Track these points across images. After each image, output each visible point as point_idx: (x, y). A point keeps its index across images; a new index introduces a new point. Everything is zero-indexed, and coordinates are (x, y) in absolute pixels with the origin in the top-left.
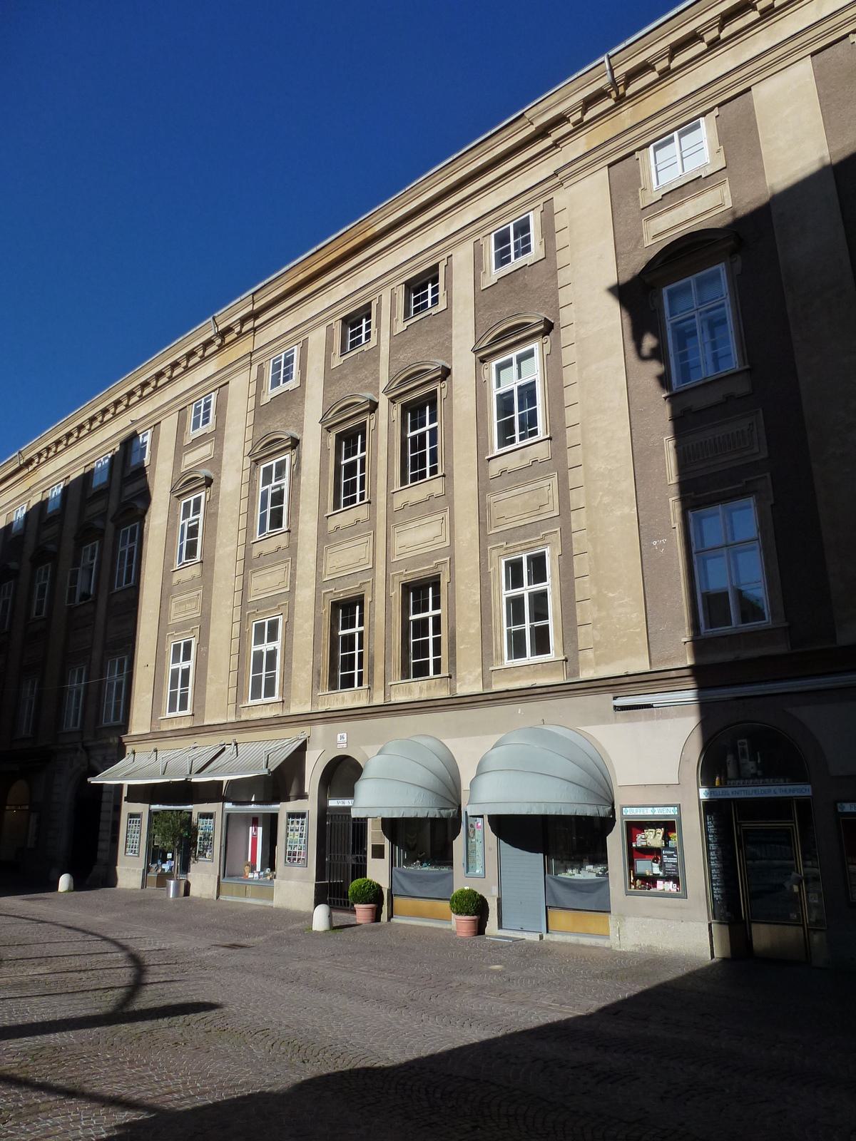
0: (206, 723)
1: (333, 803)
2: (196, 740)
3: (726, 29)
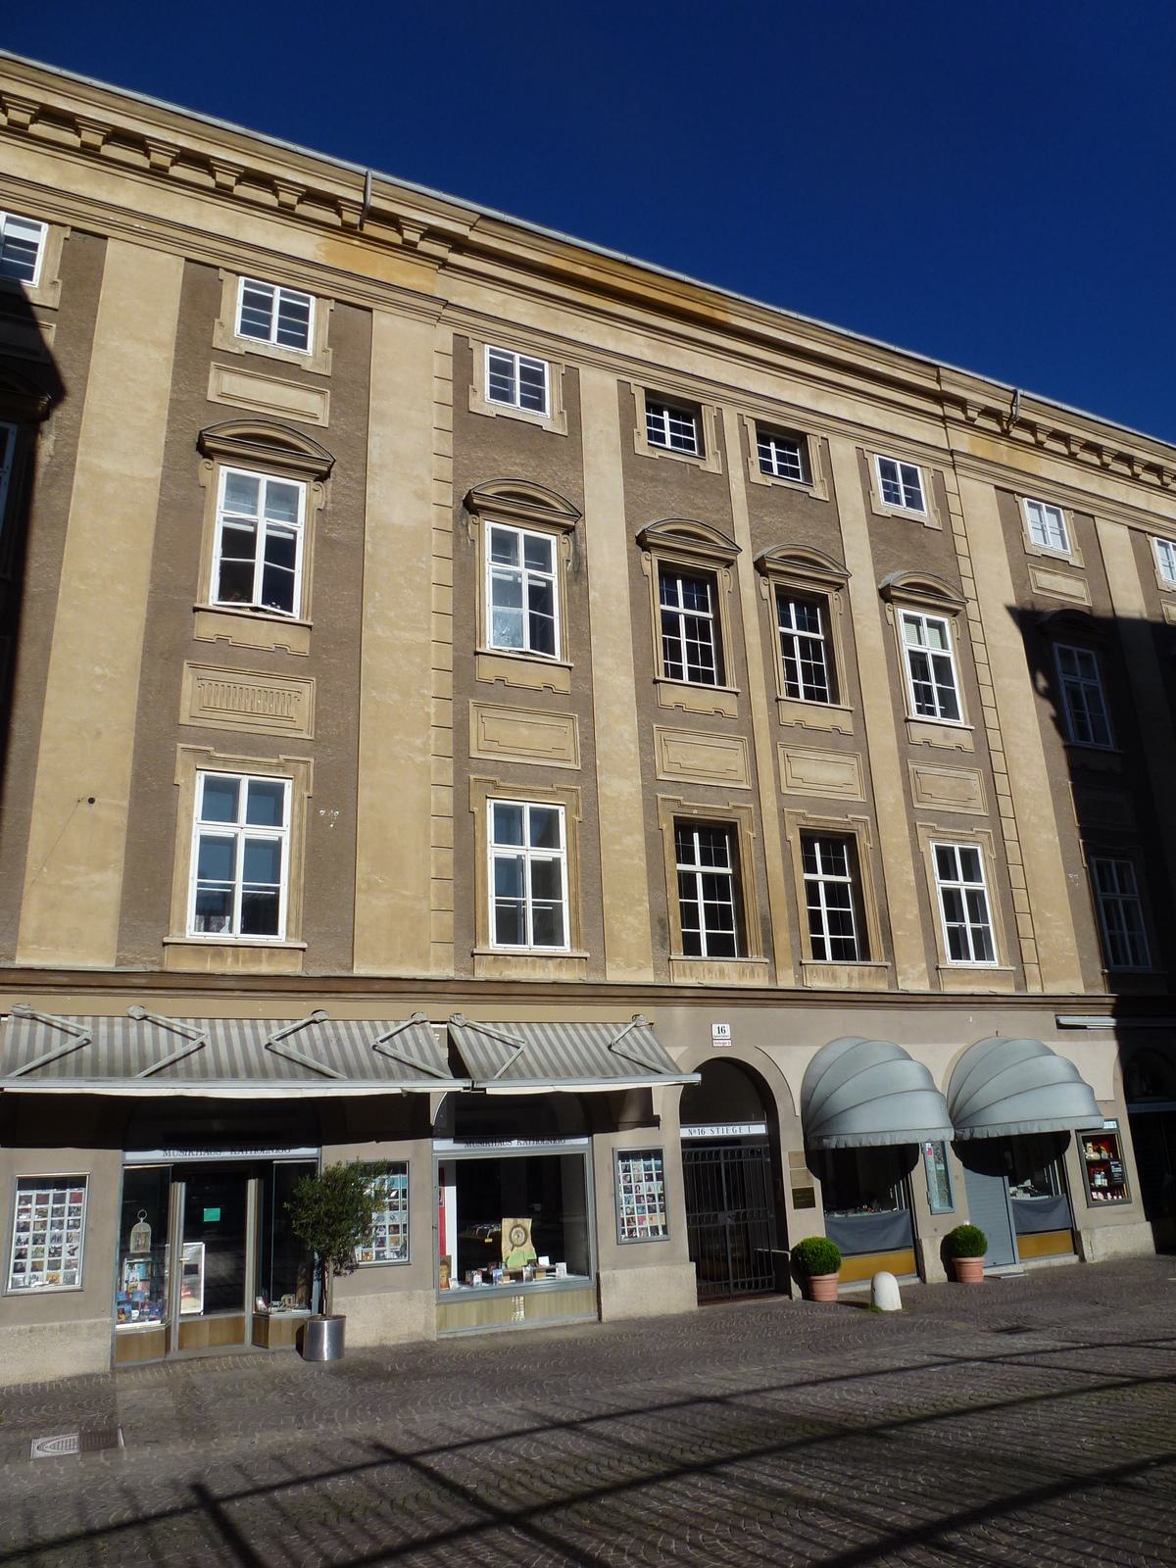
0: (358, 971)
1: (760, 1129)
2: (316, 1005)
3: (39, 126)
